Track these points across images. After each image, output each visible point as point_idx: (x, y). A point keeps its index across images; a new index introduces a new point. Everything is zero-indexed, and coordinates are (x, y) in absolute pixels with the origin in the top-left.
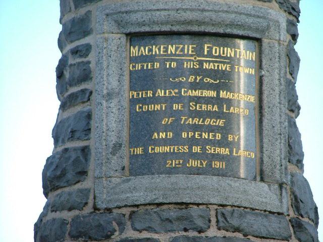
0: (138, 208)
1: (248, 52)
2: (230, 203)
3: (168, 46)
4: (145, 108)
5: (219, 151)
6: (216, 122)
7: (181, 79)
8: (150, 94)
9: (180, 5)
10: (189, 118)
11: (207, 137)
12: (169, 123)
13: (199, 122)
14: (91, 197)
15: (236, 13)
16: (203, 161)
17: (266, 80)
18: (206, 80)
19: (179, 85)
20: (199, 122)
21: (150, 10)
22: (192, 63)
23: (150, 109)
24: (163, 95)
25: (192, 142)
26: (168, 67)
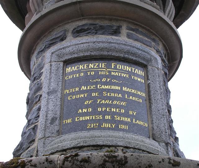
0: (66, 152)
1: (139, 71)
2: (132, 146)
3: (89, 65)
4: (74, 97)
5: (123, 119)
6: (121, 103)
7: (97, 80)
8: (77, 89)
9: (96, 40)
10: (102, 100)
11: (115, 111)
12: (89, 103)
13: (109, 102)
14: (35, 152)
15: (130, 46)
16: (112, 125)
17: (151, 86)
18: (113, 81)
19: (96, 83)
20: (109, 102)
21: (78, 44)
22: (104, 72)
23: (77, 97)
24: (85, 89)
25: (104, 113)
26: (89, 74)
